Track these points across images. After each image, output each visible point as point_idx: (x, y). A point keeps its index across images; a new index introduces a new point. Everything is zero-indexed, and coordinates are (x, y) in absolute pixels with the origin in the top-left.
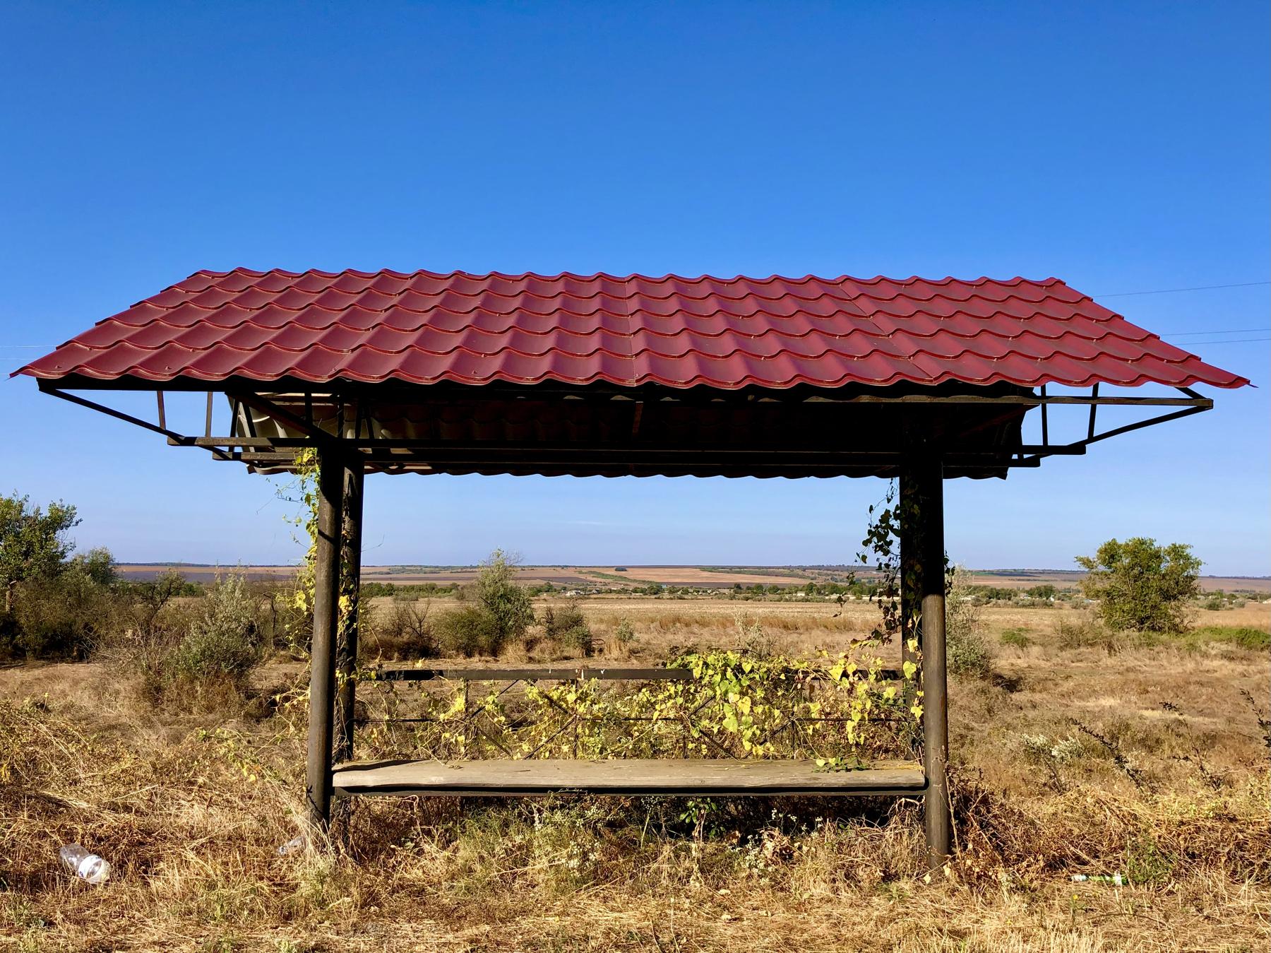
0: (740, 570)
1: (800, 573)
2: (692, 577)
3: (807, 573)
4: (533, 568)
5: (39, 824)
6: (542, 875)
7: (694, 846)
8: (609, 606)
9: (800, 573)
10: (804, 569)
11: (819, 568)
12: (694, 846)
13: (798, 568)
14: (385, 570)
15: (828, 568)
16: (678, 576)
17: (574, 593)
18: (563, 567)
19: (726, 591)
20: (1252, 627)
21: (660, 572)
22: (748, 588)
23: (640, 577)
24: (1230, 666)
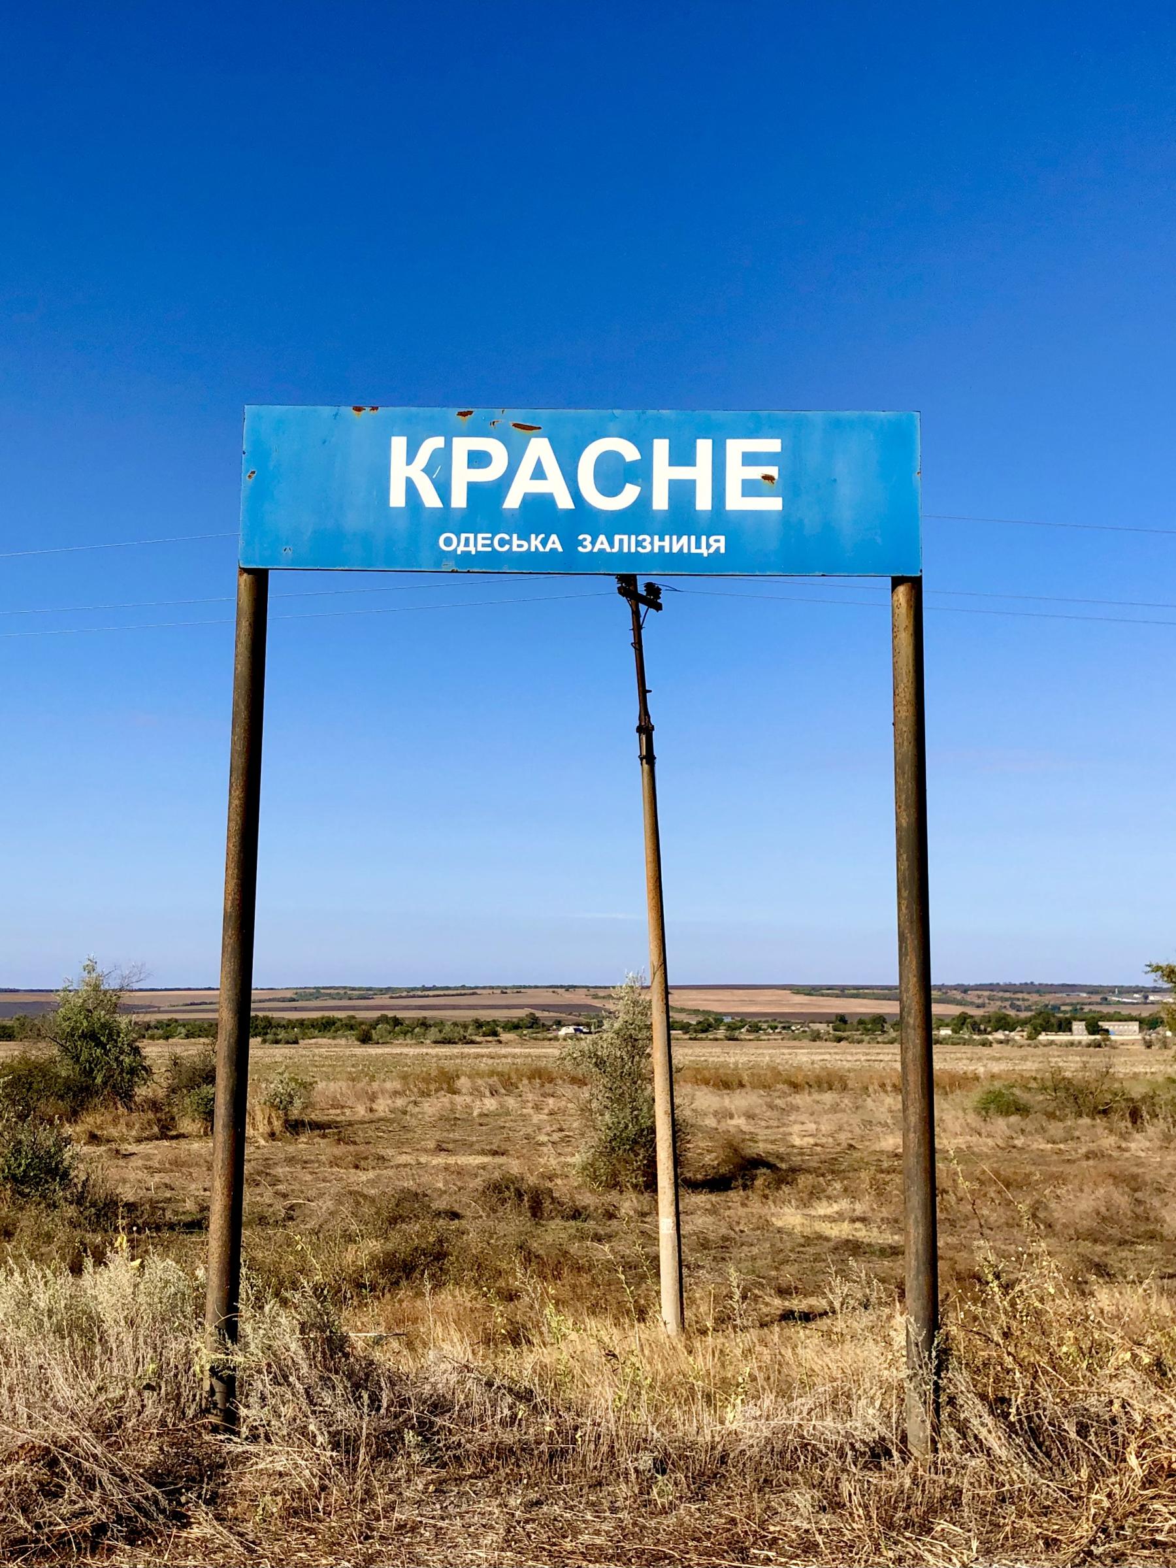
0: (842, 991)
1: (959, 996)
2: (770, 1003)
3: (971, 996)
4: (519, 989)
5: (253, 1400)
6: (1130, 1520)
7: (439, 1512)
8: (473, 1050)
9: (959, 996)
10: (965, 989)
11: (991, 987)
12: (439, 1512)
13: (956, 988)
14: (289, 995)
15: (1008, 988)
16: (753, 1002)
17: (571, 1030)
18: (568, 988)
19: (822, 1028)
20: (799, 1068)
21: (694, 994)
22: (861, 1022)
23: (691, 1005)
24: (382, 1152)
